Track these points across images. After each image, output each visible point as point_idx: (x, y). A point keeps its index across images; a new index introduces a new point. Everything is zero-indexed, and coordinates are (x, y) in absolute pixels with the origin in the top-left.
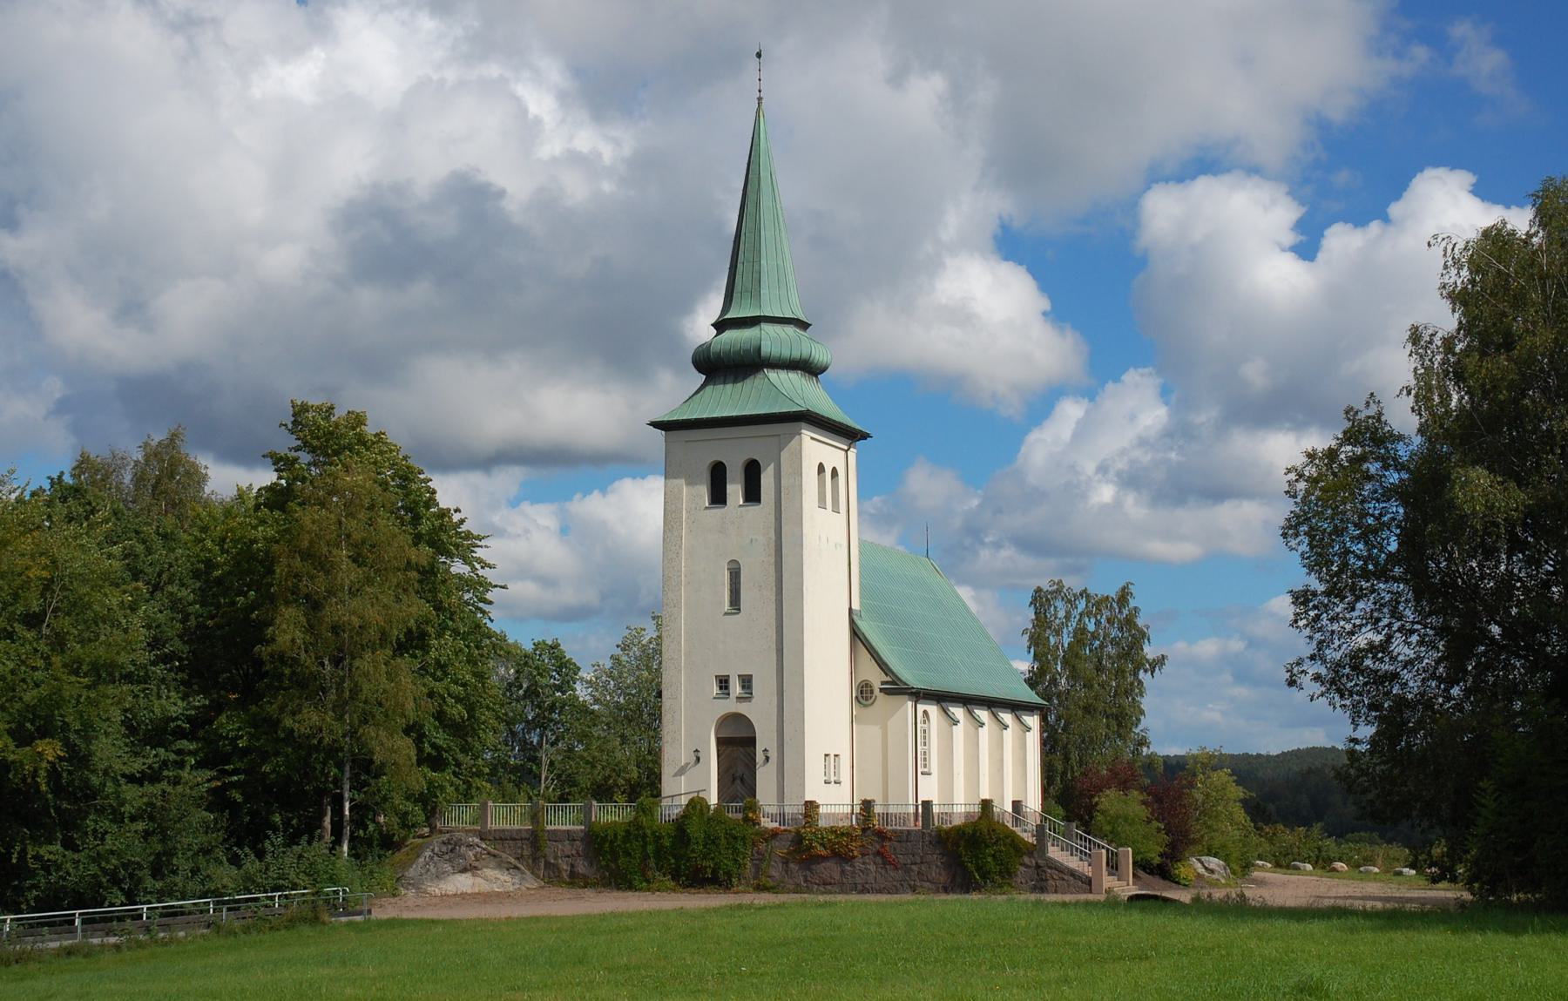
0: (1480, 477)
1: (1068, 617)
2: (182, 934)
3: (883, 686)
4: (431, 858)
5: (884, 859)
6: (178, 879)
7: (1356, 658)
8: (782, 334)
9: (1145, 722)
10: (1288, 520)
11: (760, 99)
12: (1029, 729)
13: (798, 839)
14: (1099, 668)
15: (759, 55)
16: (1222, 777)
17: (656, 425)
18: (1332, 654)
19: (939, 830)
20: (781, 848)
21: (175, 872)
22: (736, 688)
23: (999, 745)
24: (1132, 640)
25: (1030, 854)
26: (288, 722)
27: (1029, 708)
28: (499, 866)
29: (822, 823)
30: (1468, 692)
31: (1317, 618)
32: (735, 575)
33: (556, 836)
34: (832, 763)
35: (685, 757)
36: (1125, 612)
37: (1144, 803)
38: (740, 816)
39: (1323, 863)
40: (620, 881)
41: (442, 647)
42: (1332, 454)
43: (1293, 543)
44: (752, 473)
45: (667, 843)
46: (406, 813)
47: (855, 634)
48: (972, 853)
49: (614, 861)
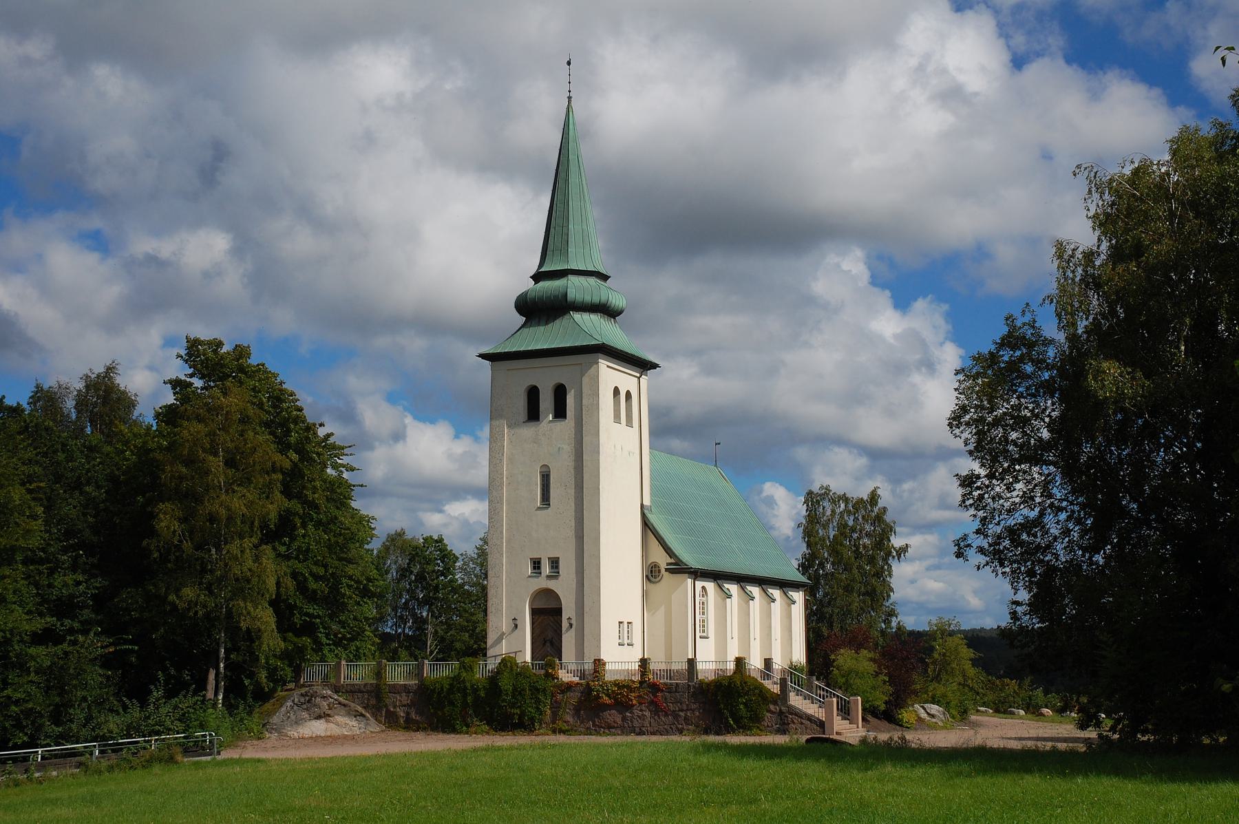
0: (1112, 369)
1: (833, 511)
2: (54, 773)
3: (666, 566)
4: (292, 707)
5: (656, 708)
6: (74, 726)
7: (1012, 532)
8: (585, 284)
9: (894, 597)
10: (954, 412)
11: (570, 98)
12: (794, 602)
13: (588, 690)
14: (858, 555)
15: (569, 63)
16: (957, 640)
17: (483, 356)
18: (994, 529)
19: (701, 682)
20: (574, 698)
21: (71, 721)
22: (546, 569)
23: (767, 615)
24: (883, 531)
25: (775, 703)
26: (172, 597)
27: (796, 586)
28: (349, 714)
29: (608, 678)
30: (1107, 558)
31: (981, 497)
32: (546, 478)
33: (395, 689)
34: (623, 631)
35: (505, 626)
36: (876, 510)
37: (871, 660)
38: (543, 672)
39: (1033, 709)
40: (445, 725)
41: (309, 536)
42: (993, 358)
43: (957, 431)
44: (560, 393)
45: (482, 694)
46: (276, 669)
47: (646, 524)
48: (728, 702)
49: (436, 710)
